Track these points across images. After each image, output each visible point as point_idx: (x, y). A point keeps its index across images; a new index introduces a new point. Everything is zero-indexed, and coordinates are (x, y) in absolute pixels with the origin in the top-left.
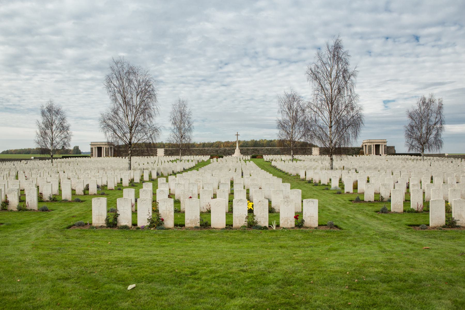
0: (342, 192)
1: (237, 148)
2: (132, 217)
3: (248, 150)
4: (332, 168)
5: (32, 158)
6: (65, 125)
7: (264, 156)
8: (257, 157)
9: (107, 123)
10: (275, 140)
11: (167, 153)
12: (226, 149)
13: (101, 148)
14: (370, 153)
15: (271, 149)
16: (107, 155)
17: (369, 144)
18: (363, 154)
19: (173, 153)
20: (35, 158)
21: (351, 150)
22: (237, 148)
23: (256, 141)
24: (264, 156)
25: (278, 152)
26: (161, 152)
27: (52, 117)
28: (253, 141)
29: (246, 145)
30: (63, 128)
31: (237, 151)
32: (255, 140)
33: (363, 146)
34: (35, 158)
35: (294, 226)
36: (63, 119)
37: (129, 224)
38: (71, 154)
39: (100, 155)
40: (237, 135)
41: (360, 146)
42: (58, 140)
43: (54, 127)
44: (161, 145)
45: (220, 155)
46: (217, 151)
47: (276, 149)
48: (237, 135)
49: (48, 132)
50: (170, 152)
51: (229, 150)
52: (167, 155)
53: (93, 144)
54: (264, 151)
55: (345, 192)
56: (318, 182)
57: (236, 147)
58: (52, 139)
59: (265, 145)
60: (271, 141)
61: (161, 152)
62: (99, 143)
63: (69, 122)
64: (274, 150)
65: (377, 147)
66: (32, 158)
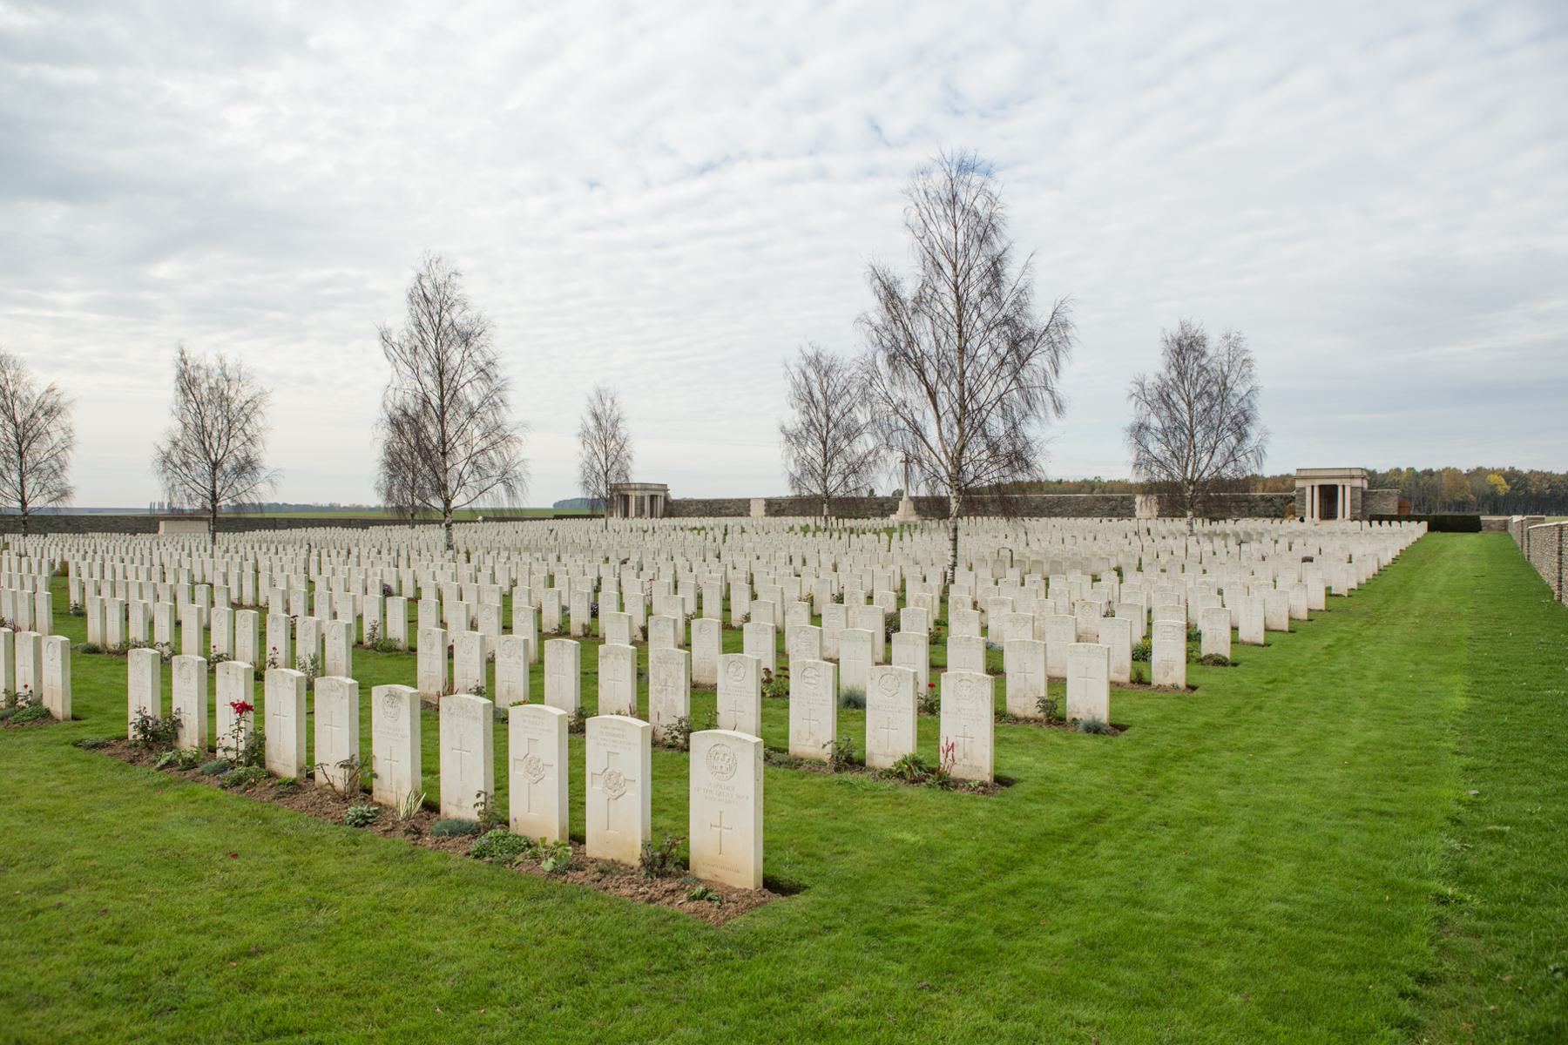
13: (1335, 487)
21: (1262, 504)
25: (1036, 507)
65: (1329, 496)
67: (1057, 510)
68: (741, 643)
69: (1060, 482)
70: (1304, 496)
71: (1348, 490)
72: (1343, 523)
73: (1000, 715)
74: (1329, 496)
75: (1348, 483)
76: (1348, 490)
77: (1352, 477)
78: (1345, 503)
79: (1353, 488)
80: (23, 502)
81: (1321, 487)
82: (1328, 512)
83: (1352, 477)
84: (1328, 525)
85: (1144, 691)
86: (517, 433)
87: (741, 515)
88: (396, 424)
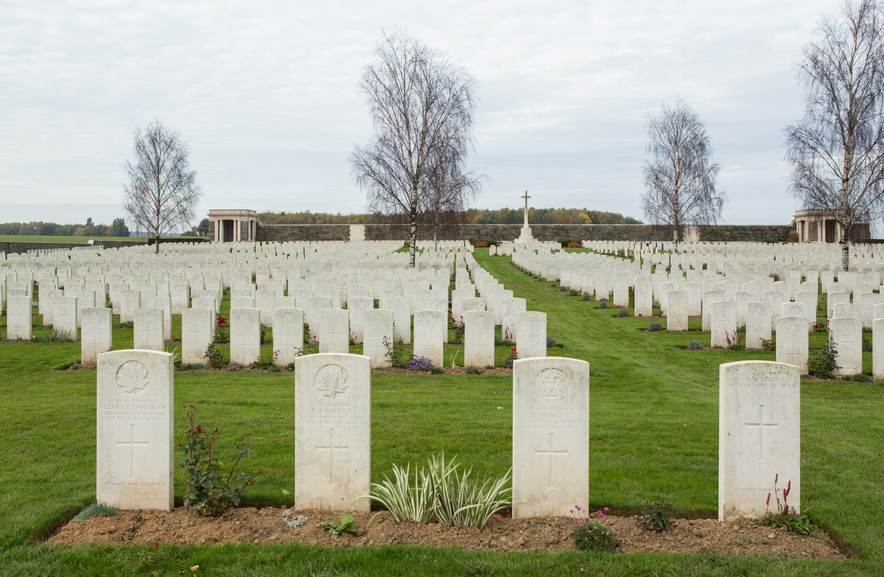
0: (630, 313)
1: (526, 224)
2: (864, 359)
3: (545, 228)
4: (846, 269)
5: (91, 242)
6: (186, 171)
7: (583, 242)
8: (570, 245)
9: (370, 168)
10: (552, 210)
11: (539, 235)
12: (497, 228)
13: (232, 221)
14: (813, 238)
15: (593, 227)
16: (244, 238)
17: (245, 219)
18: (796, 239)
19: (384, 235)
20: (96, 243)
21: (770, 232)
22: (526, 224)
23: (513, 211)
24: (583, 242)
25: (609, 234)
26: (357, 231)
27: (685, 150)
28: (505, 211)
29: (490, 219)
30: (182, 179)
31: (526, 230)
32: (511, 208)
33: (795, 224)
34: (96, 243)
35: (492, 363)
36: (180, 159)
37: (438, 359)
38: (107, 235)
39: (228, 237)
40: (526, 197)
41: (788, 222)
42: (171, 203)
43: (163, 178)
44: (307, 218)
45: (489, 239)
46: (478, 231)
47: (606, 228)
48: (526, 197)
49: (152, 185)
50: (377, 233)
51: (505, 229)
52: (372, 239)
53: (214, 213)
54: (579, 232)
55: (636, 314)
56: (591, 293)
57: (523, 222)
58: (159, 201)
59: (334, 220)
60: (545, 211)
61: (357, 231)
62: (226, 213)
63: (192, 165)
64: (600, 229)
65: (228, 225)
66: (91, 242)
67: (625, 236)
68: (374, 384)
69: (283, 214)
70: (213, 227)
71: (239, 223)
72: (235, 244)
73: (178, 365)
74: (228, 225)
75: (239, 219)
76: (239, 223)
77: (242, 215)
78: (237, 231)
79: (242, 223)
80: (677, 221)
81: (225, 222)
82: (228, 237)
83: (242, 215)
84: (228, 245)
85: (222, 373)
86: (653, 119)
87: (339, 239)
88: (358, 164)
